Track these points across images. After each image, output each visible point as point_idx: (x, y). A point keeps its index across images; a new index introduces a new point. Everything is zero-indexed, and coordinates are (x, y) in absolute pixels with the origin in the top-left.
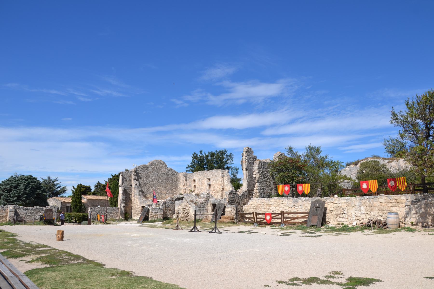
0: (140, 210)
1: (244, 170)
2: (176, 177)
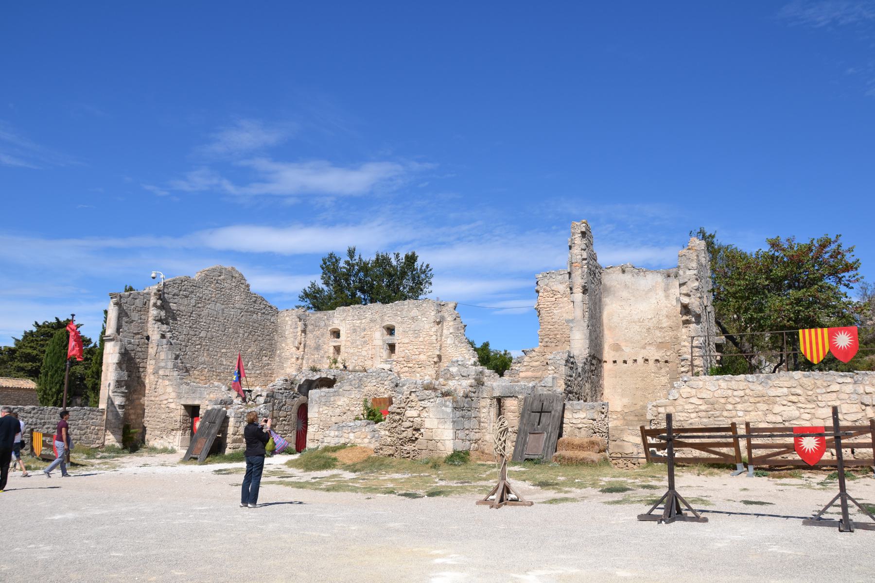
0: (178, 418)
1: (578, 290)
2: (272, 321)
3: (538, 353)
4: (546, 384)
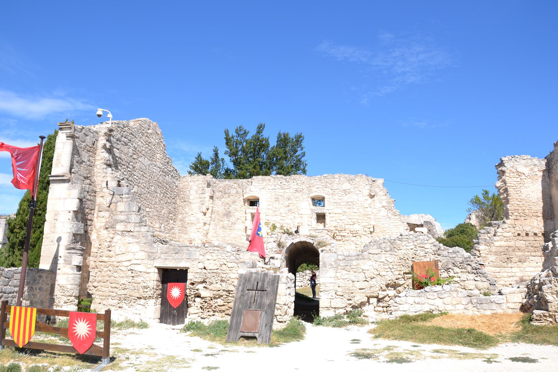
3: (509, 225)
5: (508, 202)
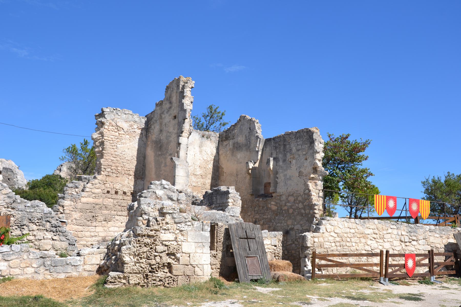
4: (234, 215)
5: (102, 156)
